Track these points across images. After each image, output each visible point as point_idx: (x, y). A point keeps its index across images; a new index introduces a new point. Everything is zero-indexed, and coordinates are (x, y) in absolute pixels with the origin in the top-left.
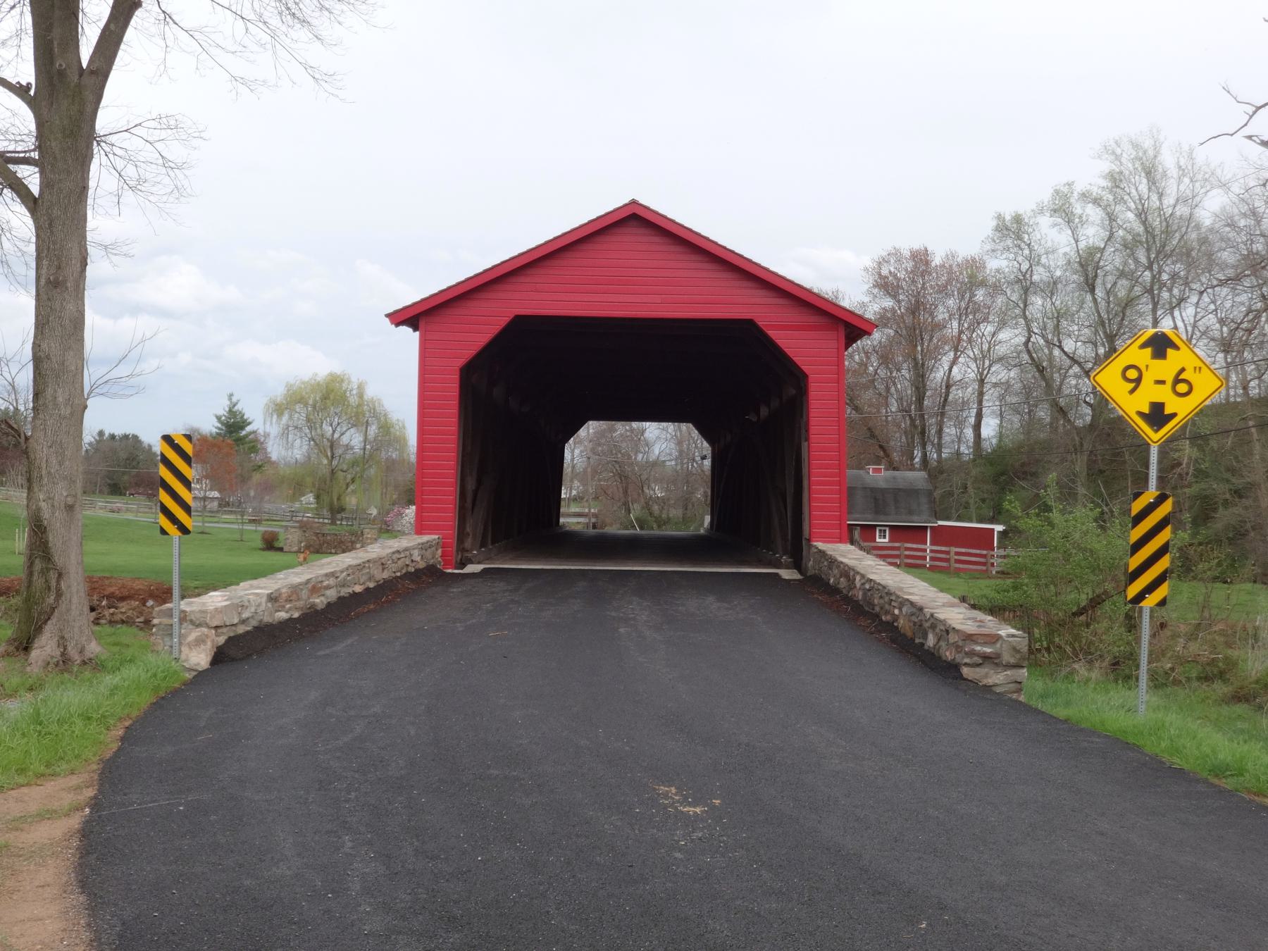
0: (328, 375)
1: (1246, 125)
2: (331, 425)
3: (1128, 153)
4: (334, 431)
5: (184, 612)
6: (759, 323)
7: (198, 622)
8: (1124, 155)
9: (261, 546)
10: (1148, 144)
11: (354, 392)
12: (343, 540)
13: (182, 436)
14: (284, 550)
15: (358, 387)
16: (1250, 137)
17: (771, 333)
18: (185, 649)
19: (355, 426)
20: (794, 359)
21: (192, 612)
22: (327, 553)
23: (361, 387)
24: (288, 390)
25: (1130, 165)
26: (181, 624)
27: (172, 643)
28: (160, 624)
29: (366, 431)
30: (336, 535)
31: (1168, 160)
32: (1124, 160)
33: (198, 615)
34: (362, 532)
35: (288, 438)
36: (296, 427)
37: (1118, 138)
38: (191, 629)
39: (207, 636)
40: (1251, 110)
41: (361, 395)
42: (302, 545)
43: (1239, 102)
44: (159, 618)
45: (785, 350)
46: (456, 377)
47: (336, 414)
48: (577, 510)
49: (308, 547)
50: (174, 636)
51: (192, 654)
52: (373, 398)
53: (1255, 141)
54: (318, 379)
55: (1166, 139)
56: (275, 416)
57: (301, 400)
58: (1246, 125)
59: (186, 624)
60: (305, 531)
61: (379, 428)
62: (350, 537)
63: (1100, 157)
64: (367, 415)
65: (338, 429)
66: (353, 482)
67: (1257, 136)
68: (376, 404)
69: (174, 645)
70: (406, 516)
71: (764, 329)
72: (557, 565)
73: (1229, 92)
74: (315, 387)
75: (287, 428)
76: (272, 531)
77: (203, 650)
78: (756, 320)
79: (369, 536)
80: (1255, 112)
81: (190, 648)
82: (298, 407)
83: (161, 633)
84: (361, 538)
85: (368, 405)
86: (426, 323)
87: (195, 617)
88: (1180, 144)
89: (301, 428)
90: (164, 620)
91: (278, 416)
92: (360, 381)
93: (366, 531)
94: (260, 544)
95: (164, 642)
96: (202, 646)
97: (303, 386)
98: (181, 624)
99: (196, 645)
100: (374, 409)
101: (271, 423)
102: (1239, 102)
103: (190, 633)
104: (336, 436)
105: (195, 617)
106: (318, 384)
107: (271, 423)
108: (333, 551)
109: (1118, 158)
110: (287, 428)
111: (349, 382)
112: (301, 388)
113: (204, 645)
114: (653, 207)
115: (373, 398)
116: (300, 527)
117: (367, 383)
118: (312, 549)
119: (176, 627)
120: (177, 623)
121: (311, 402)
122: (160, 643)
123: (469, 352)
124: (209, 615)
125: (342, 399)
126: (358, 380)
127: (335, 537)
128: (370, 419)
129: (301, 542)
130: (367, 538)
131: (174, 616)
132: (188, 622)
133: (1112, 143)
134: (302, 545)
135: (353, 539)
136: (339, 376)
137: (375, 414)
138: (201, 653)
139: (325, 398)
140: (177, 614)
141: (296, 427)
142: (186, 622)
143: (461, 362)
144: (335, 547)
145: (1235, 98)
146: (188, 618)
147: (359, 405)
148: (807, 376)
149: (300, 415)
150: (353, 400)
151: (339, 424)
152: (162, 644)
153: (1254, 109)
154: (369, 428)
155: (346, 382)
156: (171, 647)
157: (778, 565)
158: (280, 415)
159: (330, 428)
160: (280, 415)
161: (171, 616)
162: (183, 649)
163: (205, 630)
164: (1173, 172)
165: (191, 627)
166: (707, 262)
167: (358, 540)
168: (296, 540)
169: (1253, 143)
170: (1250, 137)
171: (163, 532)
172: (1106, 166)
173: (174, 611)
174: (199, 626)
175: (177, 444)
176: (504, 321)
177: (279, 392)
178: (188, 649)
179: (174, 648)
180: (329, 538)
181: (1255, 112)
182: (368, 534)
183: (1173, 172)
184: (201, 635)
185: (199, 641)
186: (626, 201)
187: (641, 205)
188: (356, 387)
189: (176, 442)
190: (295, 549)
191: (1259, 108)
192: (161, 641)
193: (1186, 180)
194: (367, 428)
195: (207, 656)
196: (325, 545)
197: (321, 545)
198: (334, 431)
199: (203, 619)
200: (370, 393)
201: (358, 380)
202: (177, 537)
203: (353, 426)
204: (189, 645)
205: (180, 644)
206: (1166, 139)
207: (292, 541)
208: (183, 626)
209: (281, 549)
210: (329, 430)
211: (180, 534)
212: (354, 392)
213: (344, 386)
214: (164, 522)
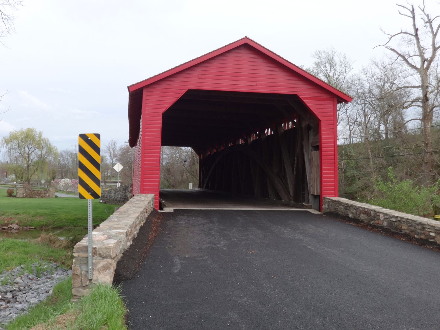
0: (27, 129)
1: (388, 42)
2: (28, 148)
3: (323, 56)
4: (29, 151)
5: (95, 248)
6: (300, 96)
7: (104, 255)
8: (322, 57)
9: (7, 195)
10: (330, 53)
11: (38, 135)
12: (41, 193)
13: (94, 135)
14: (17, 197)
15: (39, 134)
16: (387, 47)
17: (305, 101)
18: (96, 273)
19: (37, 148)
20: (315, 113)
21: (100, 248)
22: (34, 198)
23: (40, 134)
24: (11, 134)
25: (324, 60)
26: (93, 256)
27: (88, 269)
28: (78, 256)
29: (42, 151)
30: (38, 191)
31: (336, 59)
32: (322, 59)
33: (105, 251)
34: (49, 190)
35: (10, 153)
36: (14, 149)
37: (320, 50)
38: (100, 260)
39: (111, 264)
40: (390, 37)
41: (40, 137)
42: (24, 195)
43: (385, 34)
44: (77, 253)
45: (311, 109)
46: (160, 118)
47: (30, 144)
48: (114, 181)
49: (26, 196)
50: (89, 265)
51: (101, 276)
52: (45, 138)
53: (389, 49)
54: (23, 130)
55: (336, 51)
56: (5, 145)
57: (16, 138)
58: (388, 42)
59: (96, 256)
60: (25, 189)
61: (47, 150)
62: (44, 191)
63: (314, 57)
64: (42, 144)
65: (31, 149)
66: (37, 170)
67: (389, 47)
68: (46, 141)
69: (89, 271)
70: (61, 183)
71: (302, 99)
72: (193, 207)
73: (382, 30)
74: (22, 133)
75: (10, 149)
76: (11, 189)
77: (109, 273)
78: (299, 95)
79: (52, 191)
80: (391, 38)
81: (99, 272)
82: (15, 141)
83: (79, 262)
84: (48, 192)
85: (43, 140)
86: (146, 91)
87: (102, 252)
88: (340, 53)
89: (16, 149)
90: (81, 254)
91: (6, 144)
92: (40, 131)
93: (51, 189)
94: (6, 194)
95: (81, 268)
96: (107, 271)
97: (17, 133)
98: (93, 256)
99: (104, 270)
100: (45, 142)
101: (3, 147)
102: (385, 34)
103: (99, 263)
104: (30, 152)
105: (102, 252)
106: (23, 132)
107: (3, 147)
108: (37, 197)
109: (320, 58)
110: (10, 149)
111: (35, 132)
112: (16, 133)
113: (109, 270)
114: (255, 40)
115: (45, 138)
116: (23, 188)
117: (42, 132)
118: (28, 196)
119: (90, 259)
120: (91, 256)
121: (20, 139)
122: (78, 269)
123: (167, 106)
124: (112, 250)
125: (33, 139)
126: (39, 131)
127: (38, 191)
128: (44, 146)
129: (24, 194)
130: (51, 192)
131: (89, 252)
132: (98, 255)
133: (318, 52)
134: (24, 195)
135: (45, 192)
136: (31, 129)
137: (45, 143)
138: (107, 275)
139: (26, 137)
140: (91, 250)
141: (14, 149)
142: (96, 255)
143: (163, 111)
144: (38, 195)
145: (384, 33)
146: (97, 253)
147: (39, 141)
148: (321, 121)
149: (15, 145)
150: (37, 139)
151: (31, 148)
152: (80, 270)
153: (391, 36)
154: (43, 149)
155: (34, 132)
156: (88, 272)
157: (310, 207)
158: (7, 144)
159: (28, 149)
160: (7, 144)
161: (87, 251)
162: (94, 273)
163: (109, 260)
164: (338, 63)
165: (99, 258)
166: (275, 67)
167: (47, 192)
168: (22, 193)
169: (388, 49)
170: (387, 47)
171: (81, 197)
172: (316, 60)
173: (89, 248)
174: (106, 257)
175: (90, 139)
176: (183, 92)
177: (7, 134)
178: (98, 273)
179: (89, 272)
180: (35, 192)
181: (391, 38)
182: (51, 190)
183: (338, 63)
184: (106, 264)
185: (105, 268)
186: (243, 37)
187: (250, 39)
188: (38, 133)
189: (89, 138)
190: (21, 196)
191: (392, 36)
192: (79, 268)
193: (343, 66)
194: (42, 149)
195: (111, 277)
196: (34, 195)
197: (32, 195)
198: (29, 151)
199: (108, 253)
200: (44, 136)
201: (39, 131)
202: (91, 200)
203: (37, 148)
204: (99, 271)
205: (93, 269)
206: (336, 51)
207: (20, 193)
208: (94, 258)
209: (15, 196)
210: (27, 150)
211: (93, 198)
212: (38, 135)
213: (34, 133)
214: (82, 190)
